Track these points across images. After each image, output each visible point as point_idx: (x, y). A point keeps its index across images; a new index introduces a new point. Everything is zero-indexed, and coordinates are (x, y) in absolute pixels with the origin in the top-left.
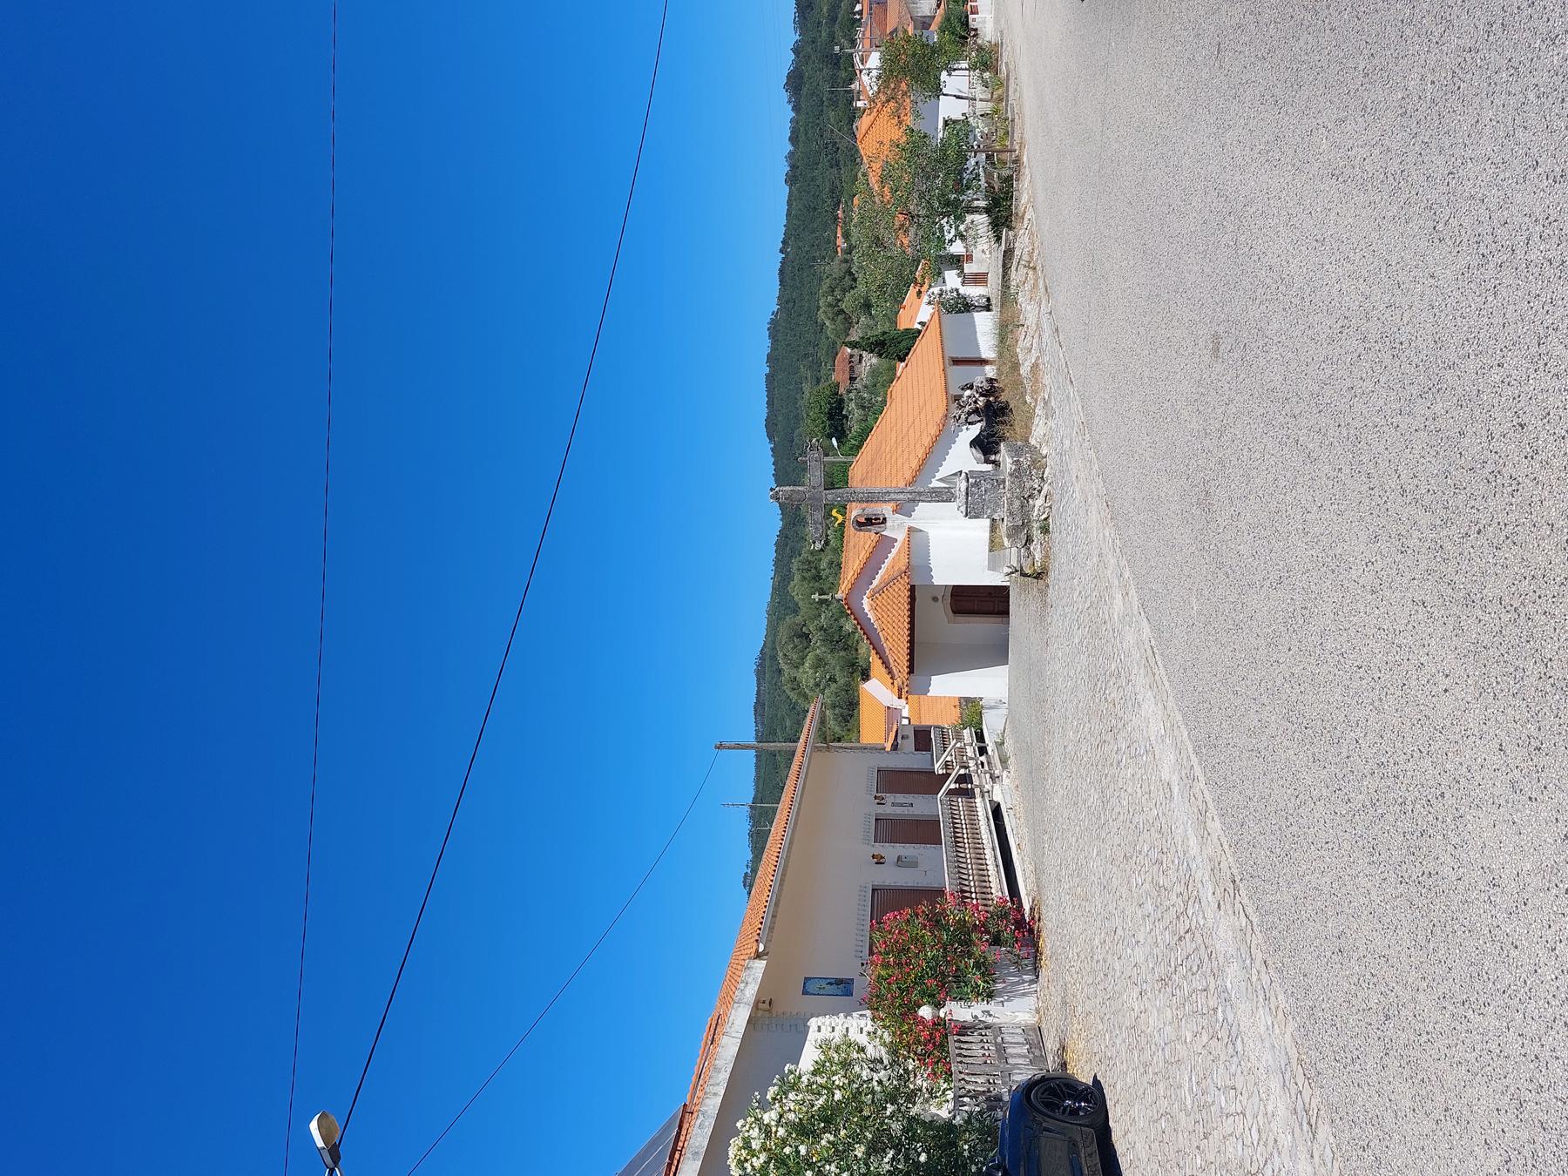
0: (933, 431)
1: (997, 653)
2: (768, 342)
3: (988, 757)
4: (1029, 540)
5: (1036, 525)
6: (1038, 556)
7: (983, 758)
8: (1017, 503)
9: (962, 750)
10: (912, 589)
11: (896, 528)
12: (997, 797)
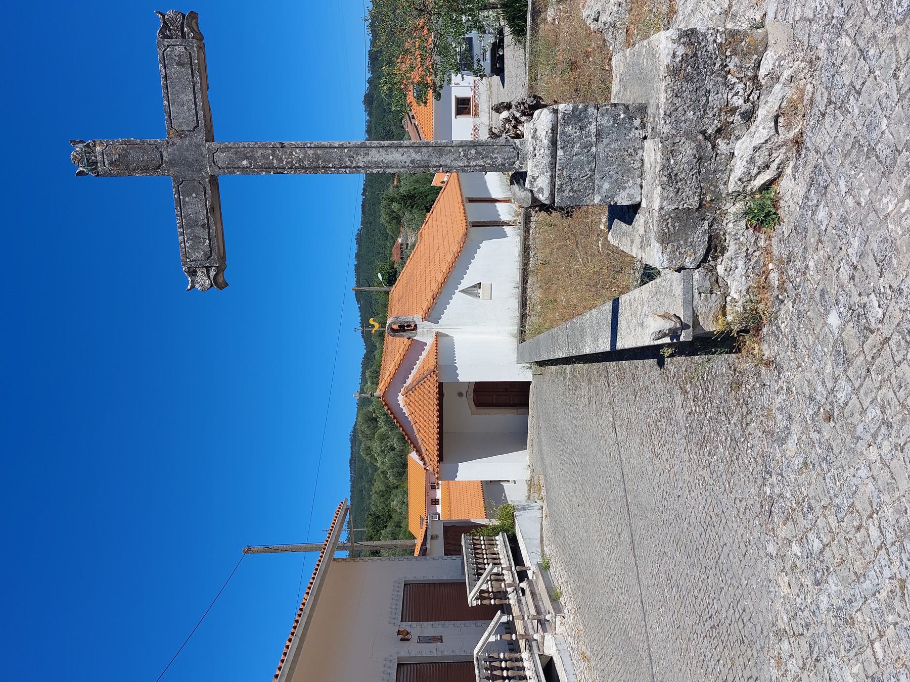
0: (455, 248)
1: (517, 440)
2: (356, 247)
3: (530, 584)
4: (714, 247)
5: (734, 209)
6: (737, 287)
7: (523, 585)
8: (688, 150)
9: (499, 578)
10: (441, 386)
11: (425, 334)
12: (550, 650)
